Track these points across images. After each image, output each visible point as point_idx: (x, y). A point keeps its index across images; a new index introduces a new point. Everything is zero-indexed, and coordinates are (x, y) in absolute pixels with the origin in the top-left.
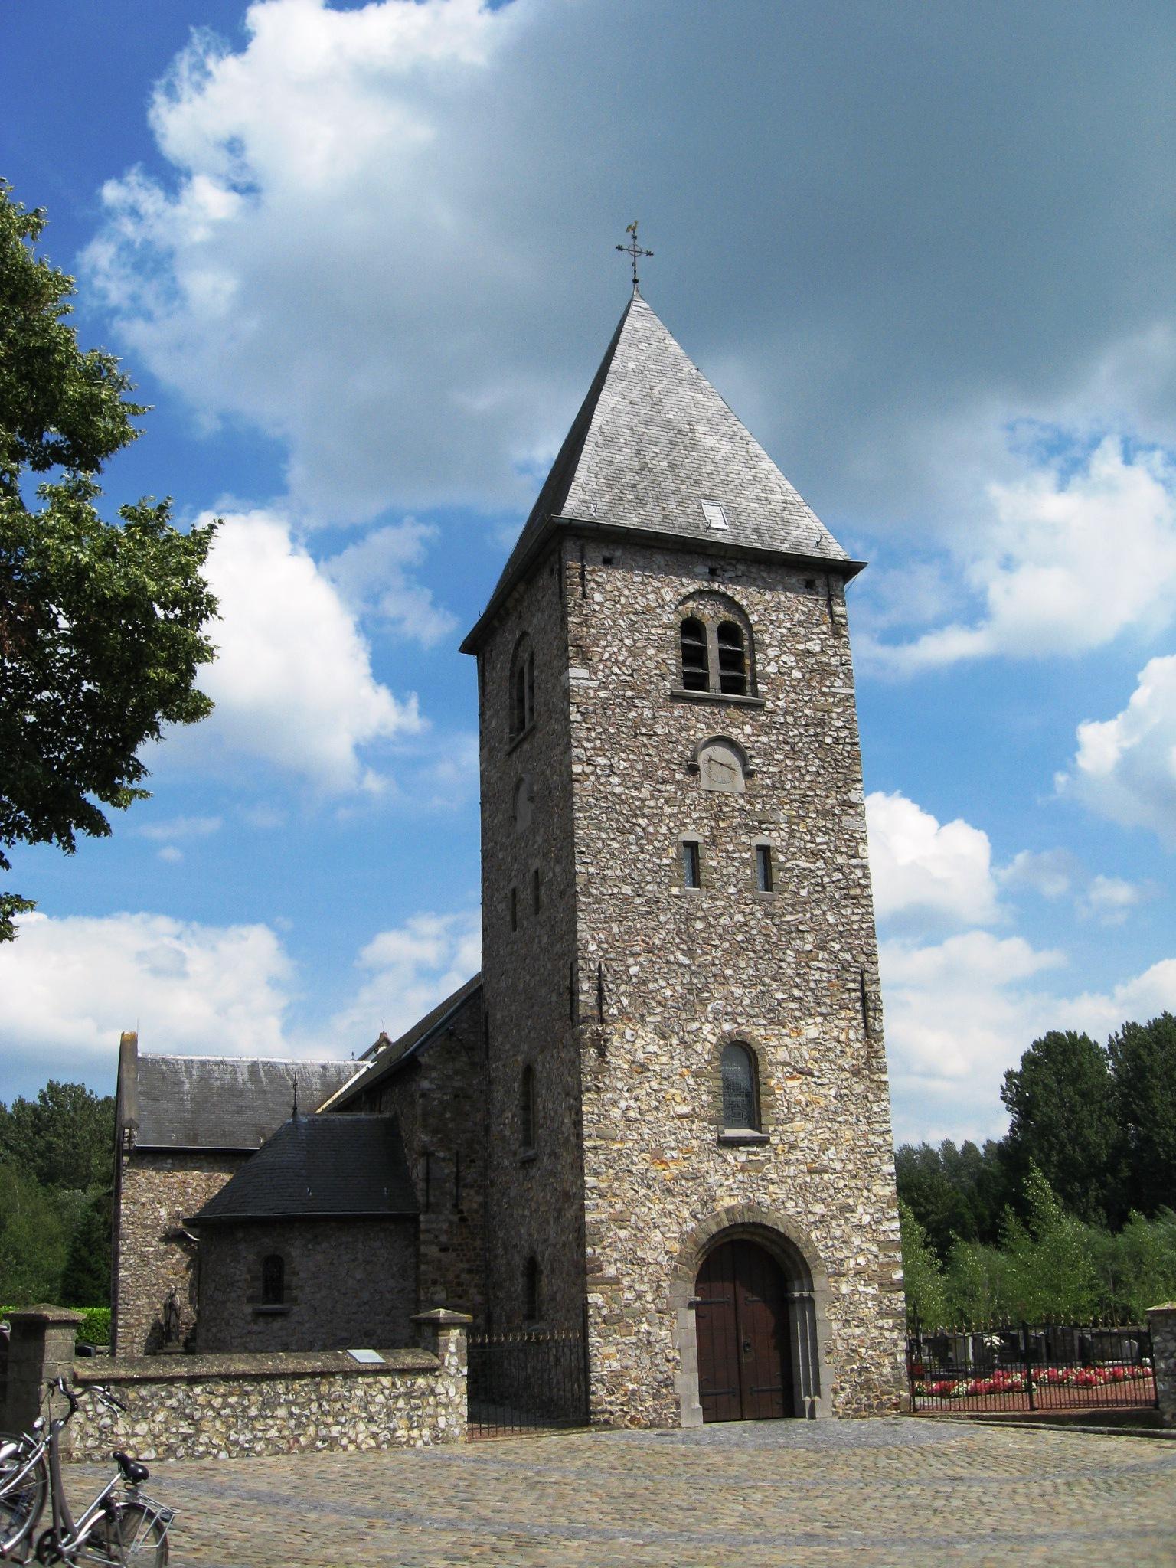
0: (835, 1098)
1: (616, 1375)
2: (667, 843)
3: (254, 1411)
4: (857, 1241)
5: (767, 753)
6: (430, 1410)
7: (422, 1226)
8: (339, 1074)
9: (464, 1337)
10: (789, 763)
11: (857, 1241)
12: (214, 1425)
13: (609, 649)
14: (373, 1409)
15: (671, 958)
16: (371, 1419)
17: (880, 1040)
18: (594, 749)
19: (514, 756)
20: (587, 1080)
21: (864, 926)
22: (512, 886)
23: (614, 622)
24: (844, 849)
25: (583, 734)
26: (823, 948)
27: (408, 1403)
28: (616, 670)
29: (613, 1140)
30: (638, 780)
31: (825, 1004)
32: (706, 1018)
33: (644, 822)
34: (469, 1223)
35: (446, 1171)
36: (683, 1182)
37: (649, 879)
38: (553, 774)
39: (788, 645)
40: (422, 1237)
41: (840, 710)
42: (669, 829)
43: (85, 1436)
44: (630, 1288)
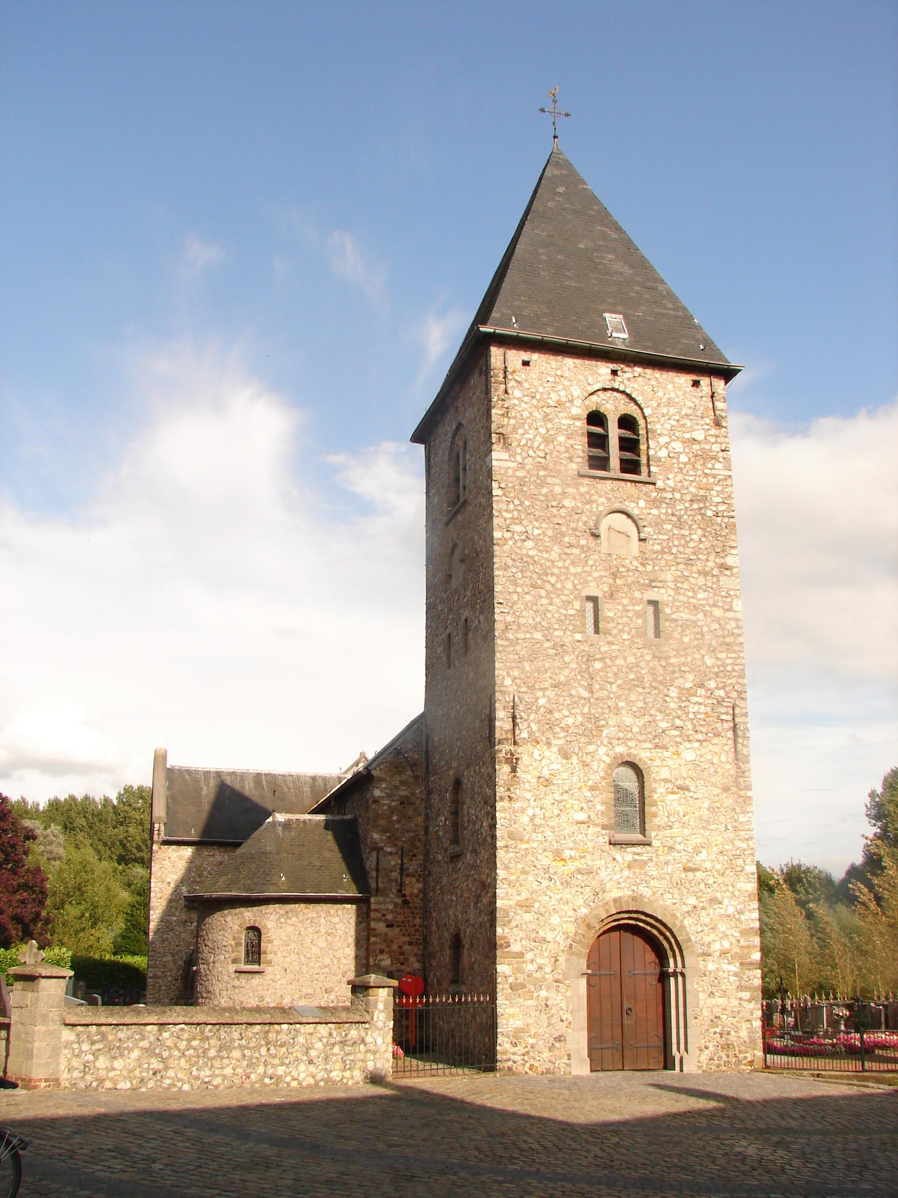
0: (708, 810)
1: (518, 1032)
2: (572, 597)
3: (212, 1053)
4: (722, 927)
5: (658, 524)
6: (361, 1056)
7: (373, 907)
8: (325, 784)
9: (392, 998)
10: (676, 532)
11: (722, 927)
12: (179, 1063)
13: (526, 436)
14: (313, 1053)
15: (573, 692)
16: (311, 1062)
17: (748, 762)
18: (512, 518)
19: (451, 526)
20: (500, 791)
21: (736, 668)
22: (447, 632)
23: (531, 414)
24: (720, 604)
25: (503, 506)
26: (701, 686)
27: (342, 1050)
28: (531, 453)
29: (522, 840)
30: (548, 544)
31: (701, 732)
32: (602, 743)
33: (553, 580)
34: (411, 905)
35: (393, 863)
36: (579, 876)
37: (556, 626)
38: (479, 540)
39: (677, 434)
40: (373, 915)
41: (719, 488)
42: (575, 586)
43: (70, 1069)
44: (532, 961)
